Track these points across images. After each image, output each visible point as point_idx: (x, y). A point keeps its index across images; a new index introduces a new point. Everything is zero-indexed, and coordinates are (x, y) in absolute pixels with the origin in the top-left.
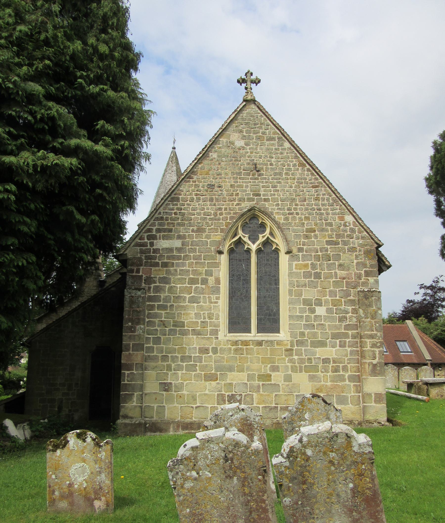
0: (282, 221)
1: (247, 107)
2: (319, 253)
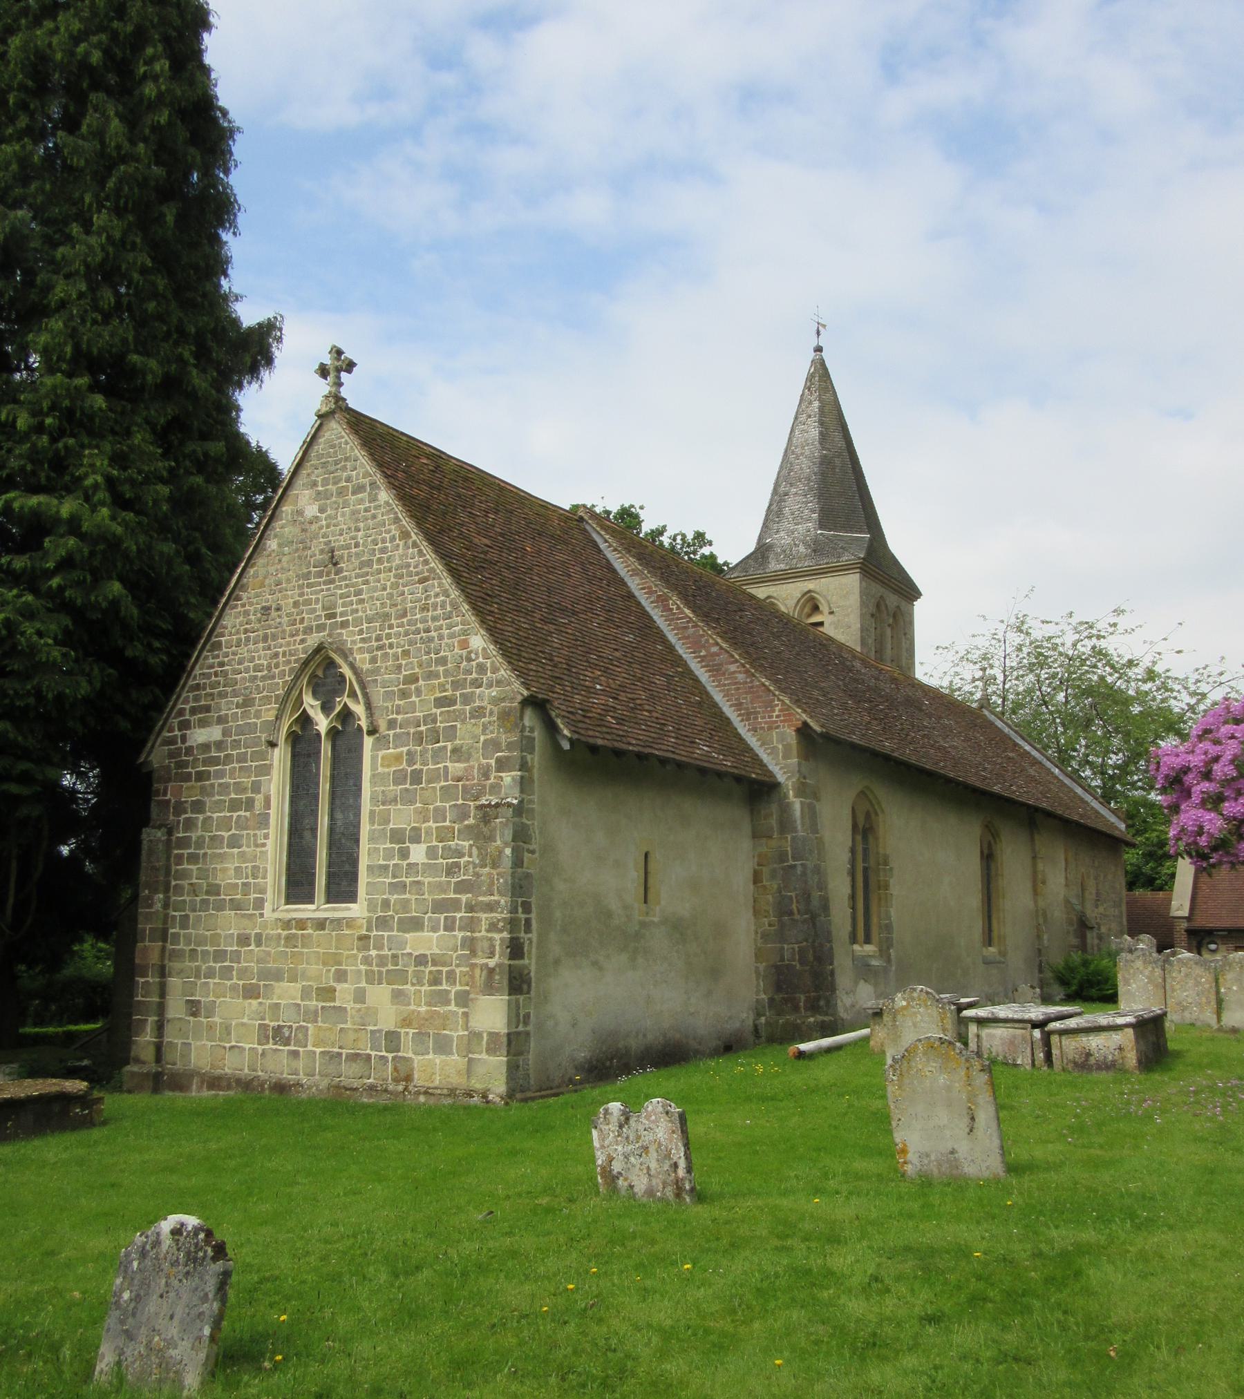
1: (325, 428)
2: (423, 728)
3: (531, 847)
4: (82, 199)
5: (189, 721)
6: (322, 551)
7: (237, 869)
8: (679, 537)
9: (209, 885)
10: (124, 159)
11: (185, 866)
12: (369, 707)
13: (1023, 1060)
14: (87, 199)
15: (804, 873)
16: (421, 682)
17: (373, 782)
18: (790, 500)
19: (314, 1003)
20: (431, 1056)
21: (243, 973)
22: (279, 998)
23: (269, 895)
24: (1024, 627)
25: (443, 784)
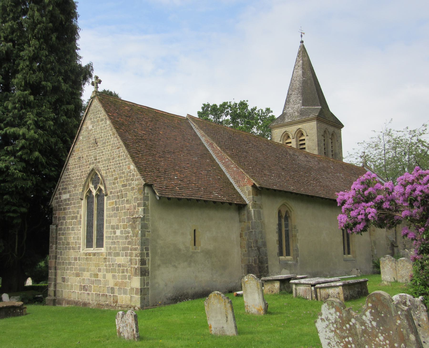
0: (105, 175)
1: (93, 101)
2: (119, 194)
3: (148, 230)
4: (28, 36)
5: (61, 192)
6: (93, 139)
7: (74, 237)
8: (260, 111)
9: (67, 242)
10: (39, 23)
11: (61, 236)
12: (105, 187)
13: (309, 297)
14: (30, 36)
15: (255, 234)
16: (118, 180)
17: (107, 211)
18: (293, 96)
19: (93, 279)
20: (122, 295)
21: (76, 269)
22: (85, 277)
23: (81, 246)
24: (390, 134)
25: (124, 211)
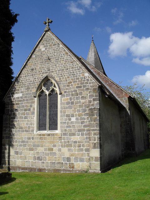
2: (73, 93)
16: (72, 83)
